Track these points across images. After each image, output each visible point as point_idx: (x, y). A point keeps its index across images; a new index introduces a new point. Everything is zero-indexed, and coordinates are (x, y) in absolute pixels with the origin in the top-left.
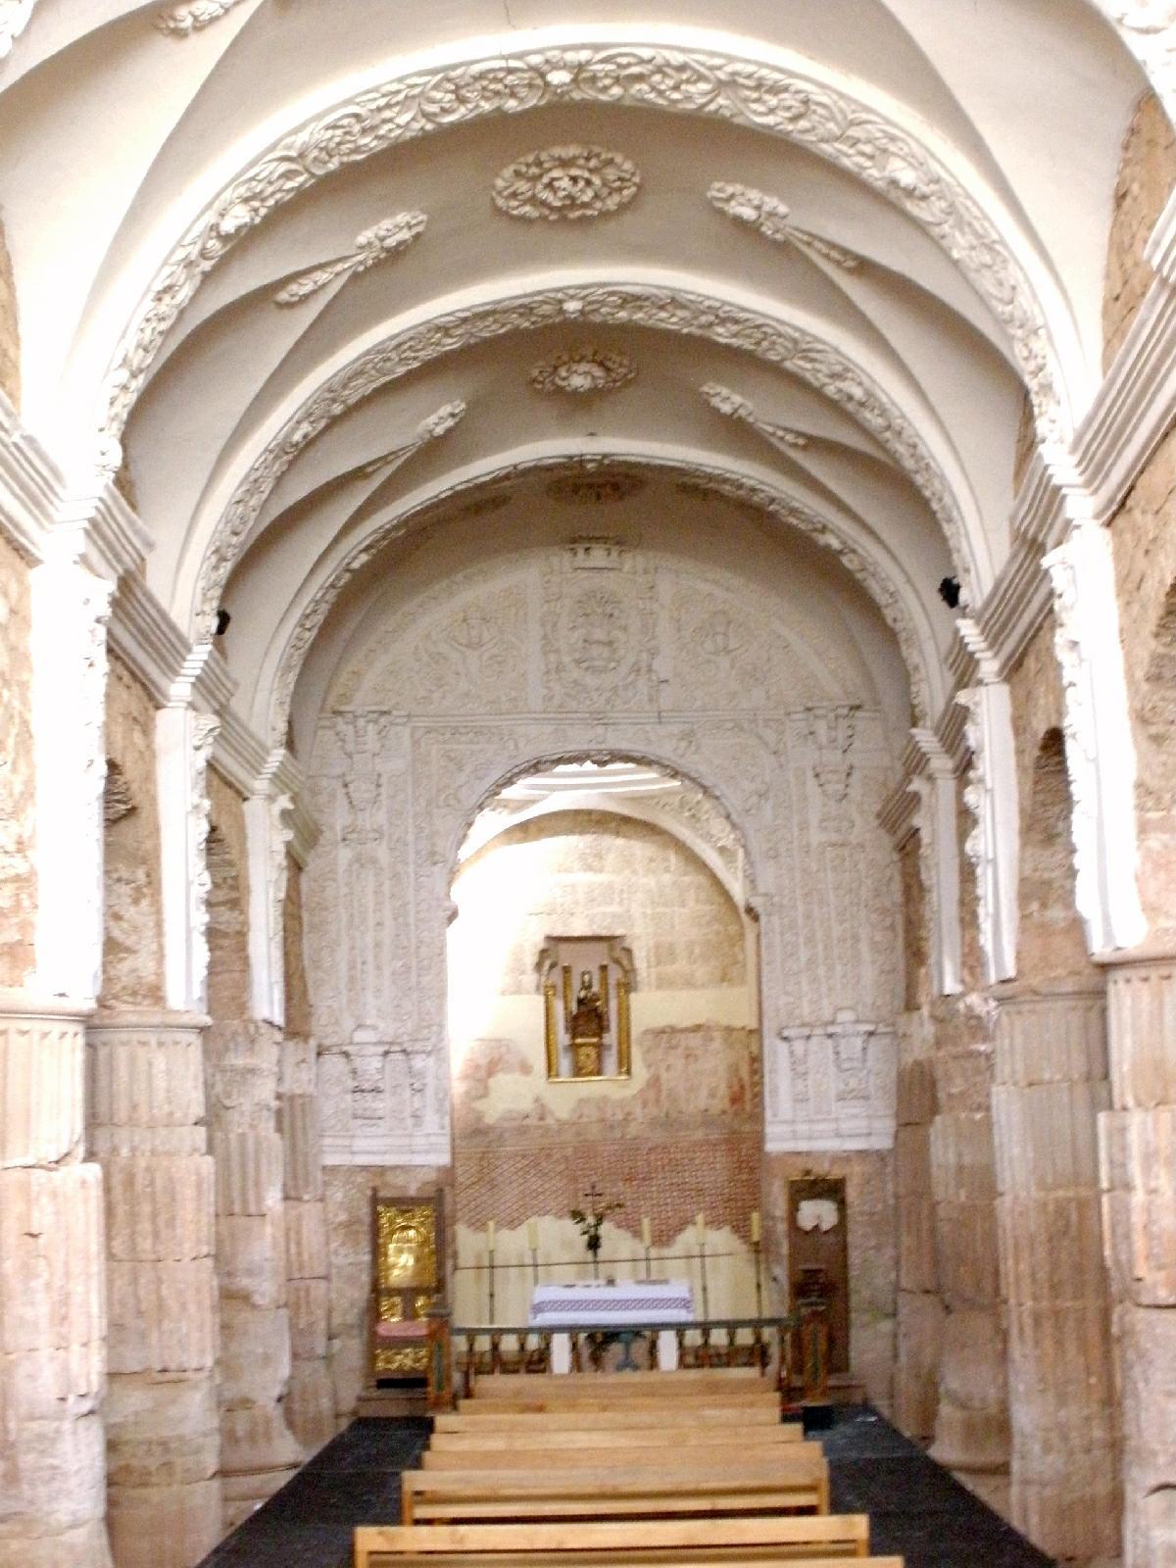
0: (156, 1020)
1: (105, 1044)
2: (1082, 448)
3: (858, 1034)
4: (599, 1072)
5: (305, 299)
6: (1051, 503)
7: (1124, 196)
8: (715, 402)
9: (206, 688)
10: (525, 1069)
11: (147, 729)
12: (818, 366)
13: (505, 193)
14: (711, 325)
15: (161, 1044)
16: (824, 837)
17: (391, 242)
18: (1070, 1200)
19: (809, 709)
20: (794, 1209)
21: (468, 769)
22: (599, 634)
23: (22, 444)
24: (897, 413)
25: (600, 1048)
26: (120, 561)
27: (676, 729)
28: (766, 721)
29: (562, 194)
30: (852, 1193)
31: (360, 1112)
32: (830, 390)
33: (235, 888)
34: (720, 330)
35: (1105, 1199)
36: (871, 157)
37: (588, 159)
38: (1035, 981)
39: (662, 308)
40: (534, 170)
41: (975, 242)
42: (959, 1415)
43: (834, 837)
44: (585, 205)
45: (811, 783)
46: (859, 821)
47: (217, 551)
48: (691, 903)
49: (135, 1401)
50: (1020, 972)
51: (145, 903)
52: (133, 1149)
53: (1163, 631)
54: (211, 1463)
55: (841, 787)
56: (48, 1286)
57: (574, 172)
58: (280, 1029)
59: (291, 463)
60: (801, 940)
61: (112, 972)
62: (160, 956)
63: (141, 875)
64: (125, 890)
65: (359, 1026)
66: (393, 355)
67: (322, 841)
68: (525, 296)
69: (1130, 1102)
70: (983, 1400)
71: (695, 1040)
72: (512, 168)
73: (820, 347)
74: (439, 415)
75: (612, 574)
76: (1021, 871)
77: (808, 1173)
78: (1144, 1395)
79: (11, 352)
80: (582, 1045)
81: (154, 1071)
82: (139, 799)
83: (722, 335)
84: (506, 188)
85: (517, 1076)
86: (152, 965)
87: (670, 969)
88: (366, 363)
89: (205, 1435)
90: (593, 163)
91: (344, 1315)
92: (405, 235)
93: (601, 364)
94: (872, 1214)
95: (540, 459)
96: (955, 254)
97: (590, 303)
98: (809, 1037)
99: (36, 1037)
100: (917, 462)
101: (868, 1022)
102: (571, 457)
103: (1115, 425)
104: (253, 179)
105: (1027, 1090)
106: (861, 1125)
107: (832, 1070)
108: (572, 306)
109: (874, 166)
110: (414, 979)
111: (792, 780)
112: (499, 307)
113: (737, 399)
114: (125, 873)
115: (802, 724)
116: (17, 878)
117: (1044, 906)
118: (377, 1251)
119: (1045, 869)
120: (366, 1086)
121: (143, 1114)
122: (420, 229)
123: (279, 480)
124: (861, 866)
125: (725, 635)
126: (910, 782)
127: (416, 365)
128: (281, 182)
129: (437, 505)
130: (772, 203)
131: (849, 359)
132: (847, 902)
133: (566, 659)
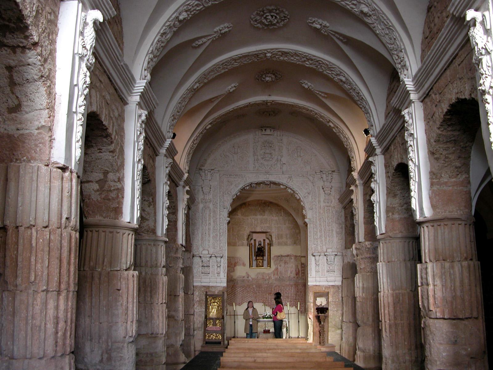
0: (153, 238)
1: (139, 244)
2: (416, 79)
4: (263, 267)
5: (200, 46)
6: (405, 96)
7: (431, 8)
8: (304, 85)
9: (169, 151)
11: (154, 161)
12: (333, 72)
13: (254, 20)
14: (305, 61)
17: (223, 31)
18: (399, 293)
19: (322, 171)
20: (315, 300)
22: (268, 151)
23: (124, 66)
24: (354, 84)
25: (263, 260)
26: (149, 107)
27: (287, 176)
29: (268, 20)
31: (203, 272)
32: (336, 79)
34: (307, 63)
35: (419, 288)
36: (355, 5)
37: (276, 10)
38: (390, 234)
39: (292, 56)
40: (262, 13)
41: (384, 27)
42: (362, 354)
44: (275, 25)
46: (333, 200)
47: (173, 116)
48: (287, 224)
49: (143, 342)
50: (386, 231)
51: (151, 207)
52: (146, 273)
53: (441, 127)
54: (164, 360)
55: (329, 191)
57: (272, 14)
59: (193, 95)
61: (142, 225)
62: (155, 221)
63: (151, 200)
64: (146, 203)
65: (204, 250)
66: (221, 66)
67: (196, 202)
68: (257, 51)
69: (428, 260)
70: (369, 350)
71: (287, 259)
72: (256, 12)
73: (334, 66)
74: (231, 86)
75: (271, 136)
76: (387, 205)
78: (432, 344)
81: (152, 252)
82: (151, 178)
83: (307, 64)
84: (254, 18)
86: (153, 224)
88: (214, 68)
89: (162, 352)
90: (277, 11)
91: (198, 324)
92: (227, 30)
93: (274, 74)
94: (335, 302)
95: (256, 101)
97: (273, 54)
98: (320, 256)
99: (121, 234)
100: (359, 98)
101: (335, 252)
102: (264, 101)
103: (429, 69)
104: (188, 5)
105: (388, 264)
106: (333, 279)
107: (326, 264)
108: (269, 55)
109: (356, 8)
110: (218, 239)
111: (317, 190)
112: (250, 54)
113: (309, 84)
114: (146, 199)
115: (320, 175)
117: (393, 214)
118: (207, 308)
119: (393, 204)
120: (205, 265)
121: (149, 264)
122: (231, 29)
123: (190, 99)
124: (334, 212)
125: (300, 152)
126: (351, 187)
127: (227, 70)
128: (196, 7)
129: (229, 112)
130: (326, 23)
131: (341, 69)
132: (330, 221)
133: (259, 158)
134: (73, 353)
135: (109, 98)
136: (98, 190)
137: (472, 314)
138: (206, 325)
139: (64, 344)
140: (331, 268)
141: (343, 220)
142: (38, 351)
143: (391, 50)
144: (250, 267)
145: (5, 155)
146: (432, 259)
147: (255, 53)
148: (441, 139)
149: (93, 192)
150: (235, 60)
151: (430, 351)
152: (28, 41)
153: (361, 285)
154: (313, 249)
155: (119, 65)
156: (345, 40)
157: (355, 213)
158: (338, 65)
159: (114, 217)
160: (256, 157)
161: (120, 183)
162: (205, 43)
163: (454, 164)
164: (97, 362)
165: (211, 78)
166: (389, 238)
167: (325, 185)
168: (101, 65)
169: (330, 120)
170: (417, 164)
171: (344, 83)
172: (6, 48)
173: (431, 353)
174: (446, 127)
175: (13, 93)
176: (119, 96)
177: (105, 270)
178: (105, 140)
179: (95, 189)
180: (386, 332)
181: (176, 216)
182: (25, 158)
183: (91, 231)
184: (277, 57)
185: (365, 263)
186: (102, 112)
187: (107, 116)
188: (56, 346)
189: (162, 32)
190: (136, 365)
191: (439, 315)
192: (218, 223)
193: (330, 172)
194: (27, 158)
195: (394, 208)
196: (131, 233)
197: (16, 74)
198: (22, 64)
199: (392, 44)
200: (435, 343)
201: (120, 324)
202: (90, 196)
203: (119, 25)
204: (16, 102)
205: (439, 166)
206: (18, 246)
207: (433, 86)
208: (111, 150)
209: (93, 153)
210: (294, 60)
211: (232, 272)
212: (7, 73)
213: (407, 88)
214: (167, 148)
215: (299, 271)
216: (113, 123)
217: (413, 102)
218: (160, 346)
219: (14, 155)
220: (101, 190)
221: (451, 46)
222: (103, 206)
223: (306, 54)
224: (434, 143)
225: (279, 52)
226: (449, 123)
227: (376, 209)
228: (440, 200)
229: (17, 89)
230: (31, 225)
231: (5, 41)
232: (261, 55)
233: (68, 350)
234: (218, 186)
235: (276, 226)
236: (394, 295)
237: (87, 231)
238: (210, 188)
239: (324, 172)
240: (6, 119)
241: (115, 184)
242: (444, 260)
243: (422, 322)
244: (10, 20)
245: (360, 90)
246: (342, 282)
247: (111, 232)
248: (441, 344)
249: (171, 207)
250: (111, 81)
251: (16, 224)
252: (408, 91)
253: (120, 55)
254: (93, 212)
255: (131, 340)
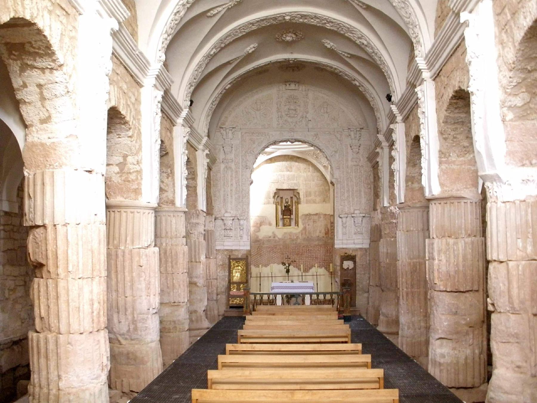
1: (159, 216)
3: (360, 217)
4: (290, 226)
5: (214, 15)
8: (326, 45)
10: (270, 224)
11: (171, 132)
12: (354, 35)
14: (325, 23)
15: (174, 216)
16: (353, 164)
18: (417, 262)
19: (349, 129)
20: (342, 263)
21: (256, 143)
22: (292, 107)
23: (139, 54)
25: (290, 219)
26: (164, 86)
27: (313, 133)
28: (337, 131)
30: (357, 259)
32: (358, 42)
33: (194, 175)
34: (328, 25)
35: (427, 262)
39: (312, 19)
42: (385, 319)
43: (355, 163)
45: (349, 148)
46: (362, 159)
47: (190, 84)
48: (316, 181)
50: (405, 201)
51: (170, 178)
52: (166, 244)
55: (357, 150)
56: (145, 280)
58: (205, 212)
60: (346, 191)
63: (169, 171)
64: (165, 175)
65: (226, 212)
66: (238, 31)
67: (216, 162)
69: (435, 237)
71: (316, 218)
73: (355, 30)
74: (250, 48)
76: (406, 174)
77: (346, 253)
78: (436, 314)
79: (136, 29)
80: (285, 218)
81: (172, 223)
83: (328, 26)
85: (268, 226)
86: (172, 195)
87: (310, 198)
88: (231, 33)
89: (185, 319)
93: (295, 34)
94: (363, 265)
96: (394, 4)
97: (292, 17)
98: (347, 217)
99: (142, 213)
101: (362, 213)
102: (286, 59)
105: (406, 233)
107: (353, 226)
108: (287, 18)
113: (332, 44)
114: (165, 170)
116: (137, 171)
117: (413, 183)
118: (230, 272)
119: (413, 173)
121: (169, 235)
125: (327, 108)
127: (244, 33)
131: (363, 33)
133: (283, 114)
134: (106, 328)
135: (126, 87)
136: (118, 173)
137: (472, 287)
138: (229, 289)
139: (99, 321)
140: (359, 230)
141: (372, 180)
142: (78, 328)
143: (408, 23)
144: (276, 226)
145: (39, 162)
146: (438, 235)
147: (273, 16)
148: (449, 121)
149: (114, 175)
150: (253, 24)
151: (434, 320)
152: (56, 64)
153: (385, 250)
154: (340, 210)
155: (134, 55)
156: (365, 7)
157: (380, 176)
158: (359, 28)
159: (134, 197)
160: (280, 113)
161: (139, 165)
162: (220, 12)
163: (463, 144)
164: (125, 332)
165: (228, 42)
166: (407, 208)
167: (353, 143)
168: (117, 59)
169: (355, 79)
170: (427, 143)
171: (366, 46)
172: (36, 70)
173: (434, 323)
174: (453, 110)
175: (44, 107)
176: (135, 81)
177: (128, 247)
178: (123, 126)
179: (116, 171)
180: (403, 299)
181: (196, 181)
182: (57, 164)
183: (113, 212)
184: (296, 19)
185: (389, 229)
186: (120, 102)
187: (125, 105)
188: (93, 323)
189: (175, 11)
190: (161, 332)
191: (442, 288)
192: (241, 184)
193: (359, 129)
194: (59, 164)
195: (414, 177)
196: (151, 211)
197: (45, 91)
198: (50, 82)
199: (408, 18)
200: (438, 314)
201: (144, 297)
202: (111, 178)
203: (133, 10)
204: (47, 115)
205: (447, 146)
206: (57, 241)
207: (442, 67)
208: (129, 135)
209: (113, 138)
210: (314, 22)
211: (257, 232)
212: (38, 90)
213: (418, 67)
214: (184, 118)
215: (328, 230)
216: (131, 110)
217: (425, 80)
218: (182, 314)
219: (47, 161)
220: (121, 171)
221: (455, 35)
222: (123, 187)
223: (326, 17)
224: (443, 124)
225: (298, 14)
226: (456, 106)
227: (396, 178)
228: (448, 179)
229: (47, 103)
230: (67, 223)
231: (36, 64)
232: (280, 18)
233: (103, 326)
234: (240, 146)
235: (304, 183)
236: (412, 264)
237: (109, 212)
238: (232, 147)
239: (351, 129)
240: (39, 130)
241: (135, 166)
242: (449, 237)
243: (429, 294)
244: (39, 48)
245: (382, 55)
246: (370, 245)
247: (132, 212)
248: (443, 314)
249: (191, 172)
250: (127, 69)
251: (54, 223)
252: (420, 70)
253: (135, 46)
254: (114, 193)
255: (155, 311)
